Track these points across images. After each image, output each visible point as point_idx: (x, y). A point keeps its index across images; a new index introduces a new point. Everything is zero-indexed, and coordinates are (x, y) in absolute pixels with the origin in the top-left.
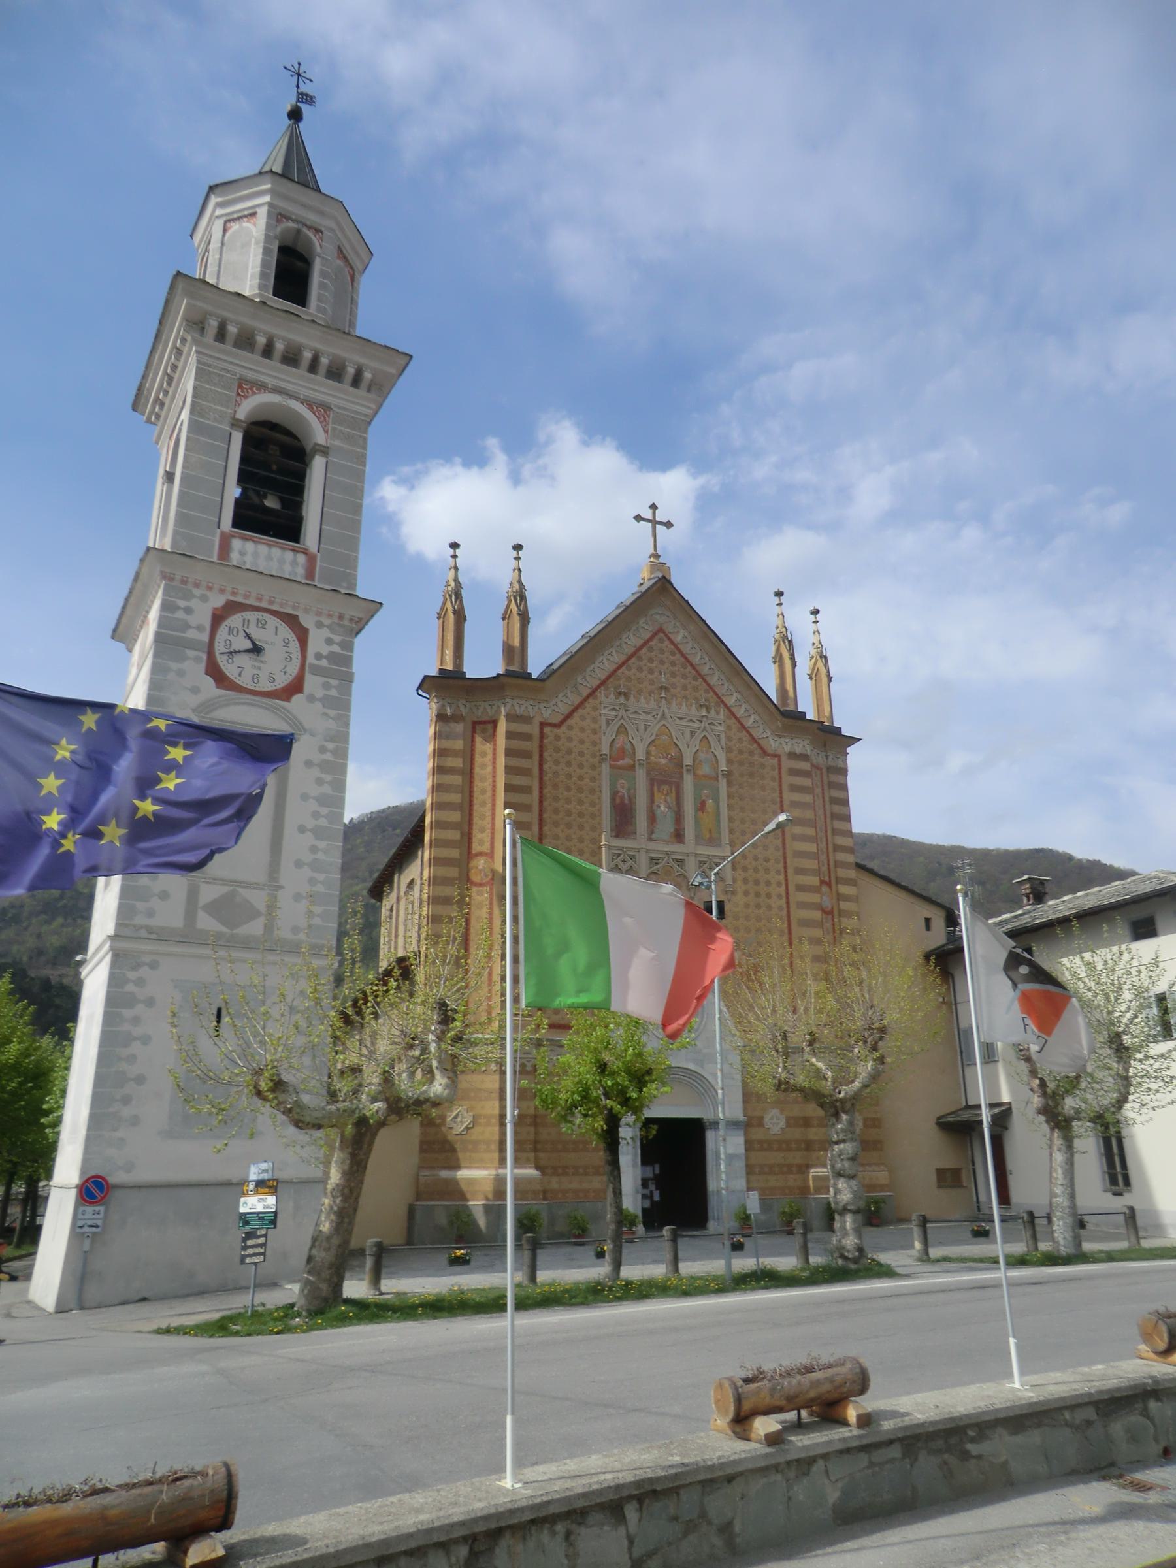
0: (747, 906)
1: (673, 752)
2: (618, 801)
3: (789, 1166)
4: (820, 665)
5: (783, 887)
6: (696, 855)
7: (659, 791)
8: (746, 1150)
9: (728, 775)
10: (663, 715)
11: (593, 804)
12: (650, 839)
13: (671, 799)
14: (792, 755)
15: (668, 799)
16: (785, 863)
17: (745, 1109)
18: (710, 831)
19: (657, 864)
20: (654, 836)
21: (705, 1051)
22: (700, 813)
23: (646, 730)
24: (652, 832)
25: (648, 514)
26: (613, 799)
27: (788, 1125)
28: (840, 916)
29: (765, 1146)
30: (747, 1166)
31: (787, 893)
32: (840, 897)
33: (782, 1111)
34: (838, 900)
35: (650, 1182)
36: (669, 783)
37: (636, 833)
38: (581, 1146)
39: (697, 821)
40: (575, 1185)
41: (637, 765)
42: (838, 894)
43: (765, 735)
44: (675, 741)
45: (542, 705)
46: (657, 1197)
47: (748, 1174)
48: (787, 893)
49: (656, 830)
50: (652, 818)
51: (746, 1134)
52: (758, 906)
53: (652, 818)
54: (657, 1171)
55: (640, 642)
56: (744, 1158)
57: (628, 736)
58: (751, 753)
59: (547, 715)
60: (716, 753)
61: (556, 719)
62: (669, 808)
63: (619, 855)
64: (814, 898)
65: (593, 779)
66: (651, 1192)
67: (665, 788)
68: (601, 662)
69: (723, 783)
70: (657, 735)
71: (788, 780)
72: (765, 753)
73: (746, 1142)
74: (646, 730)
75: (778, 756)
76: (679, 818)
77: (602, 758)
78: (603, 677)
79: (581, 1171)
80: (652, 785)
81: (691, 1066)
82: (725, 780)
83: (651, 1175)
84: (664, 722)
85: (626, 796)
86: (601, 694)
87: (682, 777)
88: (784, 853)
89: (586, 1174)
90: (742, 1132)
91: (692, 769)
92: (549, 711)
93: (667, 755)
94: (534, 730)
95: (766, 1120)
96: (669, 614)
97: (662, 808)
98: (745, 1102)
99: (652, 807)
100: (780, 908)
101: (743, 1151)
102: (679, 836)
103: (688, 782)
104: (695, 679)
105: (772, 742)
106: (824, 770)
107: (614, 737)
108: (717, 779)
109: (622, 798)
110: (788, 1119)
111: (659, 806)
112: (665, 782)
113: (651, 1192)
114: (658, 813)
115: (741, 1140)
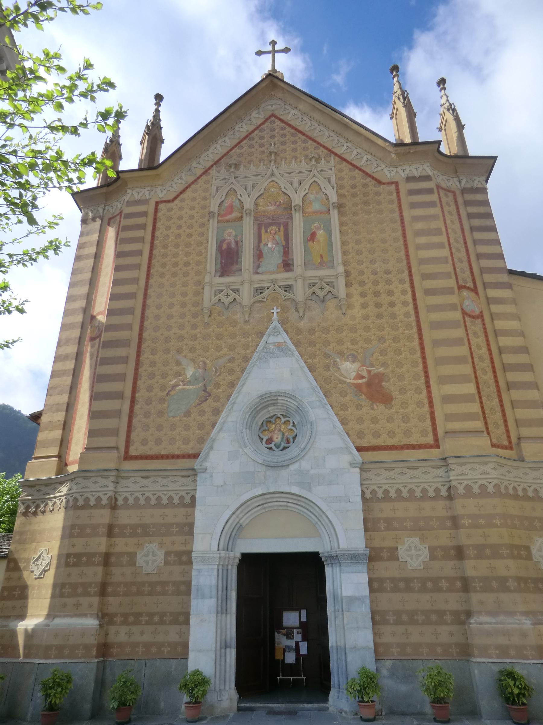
0: (366, 317)
1: (282, 199)
2: (224, 246)
3: (441, 614)
4: (449, 116)
5: (410, 295)
6: (304, 279)
7: (266, 232)
8: (372, 590)
9: (340, 207)
10: (273, 174)
11: (200, 254)
12: (257, 273)
13: (280, 237)
14: (410, 179)
15: (277, 237)
16: (410, 272)
17: (368, 540)
18: (322, 257)
19: (261, 293)
20: (260, 270)
21: (312, 472)
22: (310, 243)
23: (253, 187)
24: (259, 266)
25: (269, 48)
26: (219, 247)
27: (433, 557)
28: (492, 320)
31: (414, 300)
32: (489, 301)
33: (423, 539)
34: (489, 304)
36: (279, 225)
37: (241, 270)
39: (307, 250)
40: (147, 638)
41: (244, 215)
42: (487, 299)
43: (379, 169)
44: (283, 190)
45: (158, 190)
46: (304, 649)
47: (374, 622)
48: (414, 300)
49: (262, 265)
50: (259, 255)
51: (369, 570)
52: (379, 316)
53: (259, 255)
54: (304, 619)
55: (251, 128)
56: (368, 601)
57: (237, 196)
58: (365, 186)
59: (161, 194)
60: (327, 192)
61: (170, 198)
62: (277, 244)
63: (223, 290)
64: (453, 299)
65: (201, 234)
66: (297, 644)
67: (273, 228)
68: (216, 148)
69: (335, 215)
70: (265, 190)
71: (405, 200)
72: (380, 182)
73: (371, 581)
74: (253, 187)
75: (396, 184)
76: (287, 250)
77: (211, 215)
78: (216, 159)
80: (259, 229)
81: (295, 490)
82: (336, 212)
83: (297, 624)
84: (273, 178)
85: (233, 242)
86: (213, 172)
87: (291, 217)
88: (409, 263)
89: (162, 622)
91: (302, 208)
92: (164, 192)
93: (276, 203)
94: (151, 209)
96: (279, 102)
97: (270, 245)
99: (259, 246)
100: (407, 315)
101: (367, 593)
102: (287, 266)
103: (297, 220)
104: (304, 142)
105: (387, 173)
106: (458, 193)
107: (223, 199)
108: (328, 212)
109: (229, 244)
110: (432, 550)
111: (266, 244)
112: (271, 224)
113: (297, 644)
114: (265, 250)
115: (363, 578)
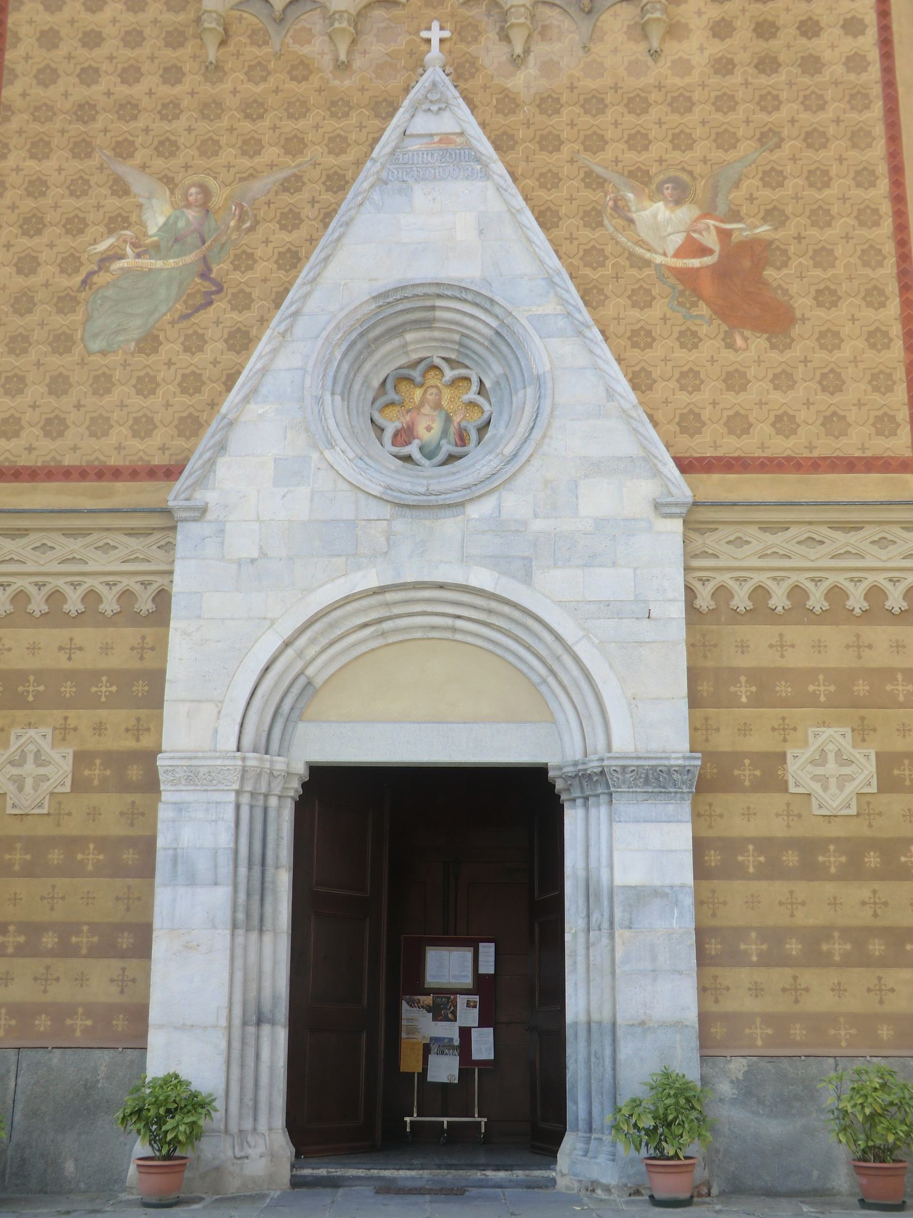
21: (538, 525)
29: (872, 860)
30: (702, 934)
33: (862, 733)
35: (461, 1000)
38: (55, 856)
47: (703, 959)
51: (696, 816)
54: (487, 966)
56: (688, 901)
66: (465, 1033)
73: (699, 846)
79: (49, 940)
81: (482, 578)
83: (467, 981)
89: (66, 950)
90: (686, 809)
95: (792, 766)
98: (694, 701)
100: (855, 62)
101: (688, 877)
110: (81, 758)
113: (465, 1033)
